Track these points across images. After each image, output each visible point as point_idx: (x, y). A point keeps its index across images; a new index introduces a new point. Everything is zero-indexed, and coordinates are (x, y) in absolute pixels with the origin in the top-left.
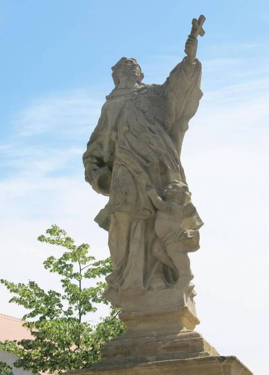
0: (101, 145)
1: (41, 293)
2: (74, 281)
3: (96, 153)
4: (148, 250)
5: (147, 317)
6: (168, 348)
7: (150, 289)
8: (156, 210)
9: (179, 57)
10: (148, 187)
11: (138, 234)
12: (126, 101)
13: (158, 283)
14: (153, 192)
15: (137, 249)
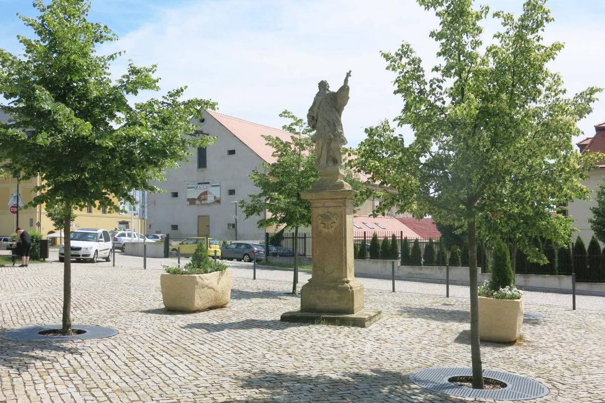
0: (313, 112)
1: (282, 143)
2: (296, 136)
3: (312, 115)
4: (328, 152)
5: (327, 175)
6: (333, 186)
7: (328, 166)
8: (331, 140)
9: (342, 84)
10: (329, 132)
11: (325, 147)
12: (322, 98)
13: (331, 164)
14: (330, 134)
15: (324, 153)
